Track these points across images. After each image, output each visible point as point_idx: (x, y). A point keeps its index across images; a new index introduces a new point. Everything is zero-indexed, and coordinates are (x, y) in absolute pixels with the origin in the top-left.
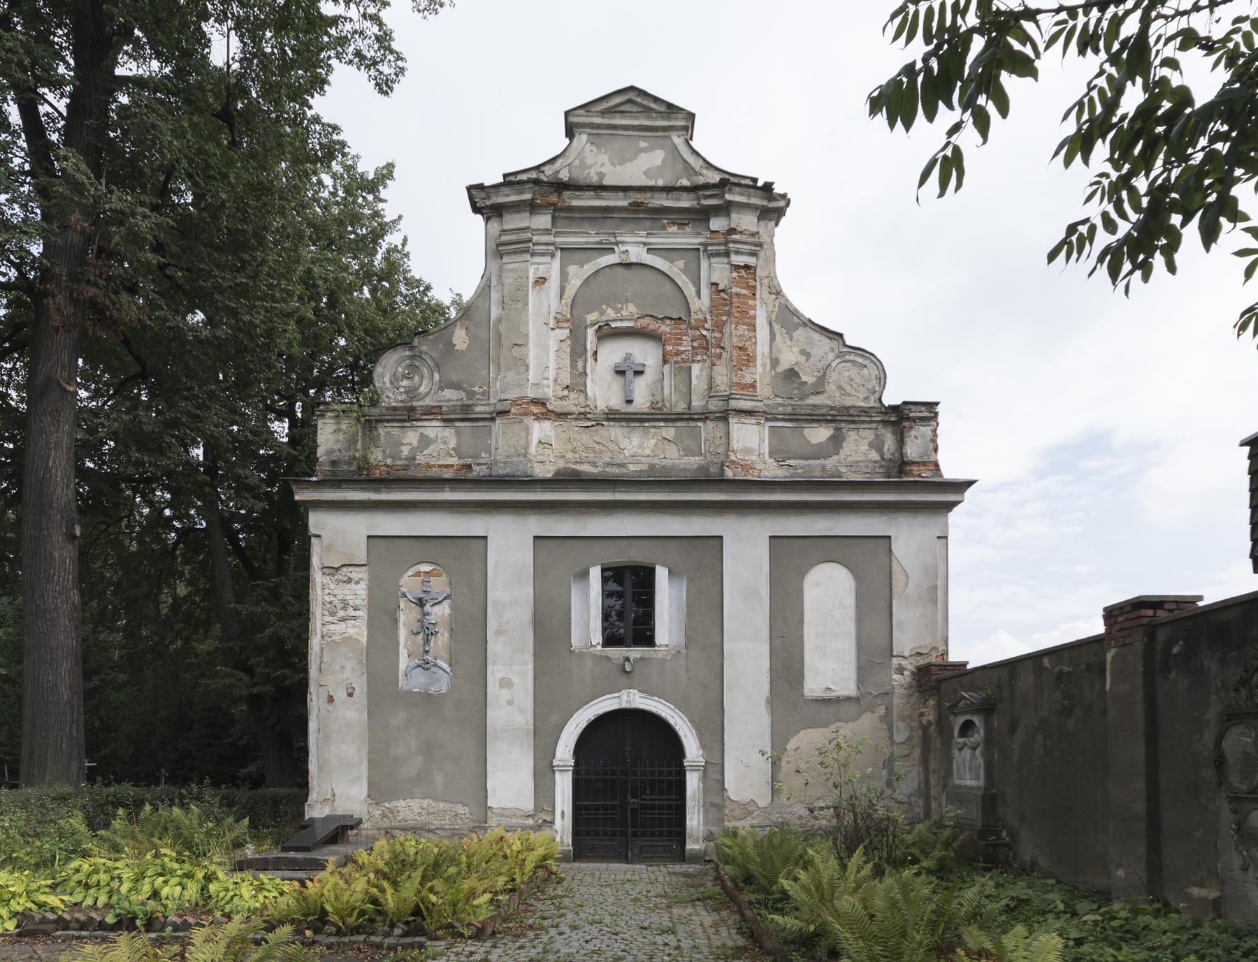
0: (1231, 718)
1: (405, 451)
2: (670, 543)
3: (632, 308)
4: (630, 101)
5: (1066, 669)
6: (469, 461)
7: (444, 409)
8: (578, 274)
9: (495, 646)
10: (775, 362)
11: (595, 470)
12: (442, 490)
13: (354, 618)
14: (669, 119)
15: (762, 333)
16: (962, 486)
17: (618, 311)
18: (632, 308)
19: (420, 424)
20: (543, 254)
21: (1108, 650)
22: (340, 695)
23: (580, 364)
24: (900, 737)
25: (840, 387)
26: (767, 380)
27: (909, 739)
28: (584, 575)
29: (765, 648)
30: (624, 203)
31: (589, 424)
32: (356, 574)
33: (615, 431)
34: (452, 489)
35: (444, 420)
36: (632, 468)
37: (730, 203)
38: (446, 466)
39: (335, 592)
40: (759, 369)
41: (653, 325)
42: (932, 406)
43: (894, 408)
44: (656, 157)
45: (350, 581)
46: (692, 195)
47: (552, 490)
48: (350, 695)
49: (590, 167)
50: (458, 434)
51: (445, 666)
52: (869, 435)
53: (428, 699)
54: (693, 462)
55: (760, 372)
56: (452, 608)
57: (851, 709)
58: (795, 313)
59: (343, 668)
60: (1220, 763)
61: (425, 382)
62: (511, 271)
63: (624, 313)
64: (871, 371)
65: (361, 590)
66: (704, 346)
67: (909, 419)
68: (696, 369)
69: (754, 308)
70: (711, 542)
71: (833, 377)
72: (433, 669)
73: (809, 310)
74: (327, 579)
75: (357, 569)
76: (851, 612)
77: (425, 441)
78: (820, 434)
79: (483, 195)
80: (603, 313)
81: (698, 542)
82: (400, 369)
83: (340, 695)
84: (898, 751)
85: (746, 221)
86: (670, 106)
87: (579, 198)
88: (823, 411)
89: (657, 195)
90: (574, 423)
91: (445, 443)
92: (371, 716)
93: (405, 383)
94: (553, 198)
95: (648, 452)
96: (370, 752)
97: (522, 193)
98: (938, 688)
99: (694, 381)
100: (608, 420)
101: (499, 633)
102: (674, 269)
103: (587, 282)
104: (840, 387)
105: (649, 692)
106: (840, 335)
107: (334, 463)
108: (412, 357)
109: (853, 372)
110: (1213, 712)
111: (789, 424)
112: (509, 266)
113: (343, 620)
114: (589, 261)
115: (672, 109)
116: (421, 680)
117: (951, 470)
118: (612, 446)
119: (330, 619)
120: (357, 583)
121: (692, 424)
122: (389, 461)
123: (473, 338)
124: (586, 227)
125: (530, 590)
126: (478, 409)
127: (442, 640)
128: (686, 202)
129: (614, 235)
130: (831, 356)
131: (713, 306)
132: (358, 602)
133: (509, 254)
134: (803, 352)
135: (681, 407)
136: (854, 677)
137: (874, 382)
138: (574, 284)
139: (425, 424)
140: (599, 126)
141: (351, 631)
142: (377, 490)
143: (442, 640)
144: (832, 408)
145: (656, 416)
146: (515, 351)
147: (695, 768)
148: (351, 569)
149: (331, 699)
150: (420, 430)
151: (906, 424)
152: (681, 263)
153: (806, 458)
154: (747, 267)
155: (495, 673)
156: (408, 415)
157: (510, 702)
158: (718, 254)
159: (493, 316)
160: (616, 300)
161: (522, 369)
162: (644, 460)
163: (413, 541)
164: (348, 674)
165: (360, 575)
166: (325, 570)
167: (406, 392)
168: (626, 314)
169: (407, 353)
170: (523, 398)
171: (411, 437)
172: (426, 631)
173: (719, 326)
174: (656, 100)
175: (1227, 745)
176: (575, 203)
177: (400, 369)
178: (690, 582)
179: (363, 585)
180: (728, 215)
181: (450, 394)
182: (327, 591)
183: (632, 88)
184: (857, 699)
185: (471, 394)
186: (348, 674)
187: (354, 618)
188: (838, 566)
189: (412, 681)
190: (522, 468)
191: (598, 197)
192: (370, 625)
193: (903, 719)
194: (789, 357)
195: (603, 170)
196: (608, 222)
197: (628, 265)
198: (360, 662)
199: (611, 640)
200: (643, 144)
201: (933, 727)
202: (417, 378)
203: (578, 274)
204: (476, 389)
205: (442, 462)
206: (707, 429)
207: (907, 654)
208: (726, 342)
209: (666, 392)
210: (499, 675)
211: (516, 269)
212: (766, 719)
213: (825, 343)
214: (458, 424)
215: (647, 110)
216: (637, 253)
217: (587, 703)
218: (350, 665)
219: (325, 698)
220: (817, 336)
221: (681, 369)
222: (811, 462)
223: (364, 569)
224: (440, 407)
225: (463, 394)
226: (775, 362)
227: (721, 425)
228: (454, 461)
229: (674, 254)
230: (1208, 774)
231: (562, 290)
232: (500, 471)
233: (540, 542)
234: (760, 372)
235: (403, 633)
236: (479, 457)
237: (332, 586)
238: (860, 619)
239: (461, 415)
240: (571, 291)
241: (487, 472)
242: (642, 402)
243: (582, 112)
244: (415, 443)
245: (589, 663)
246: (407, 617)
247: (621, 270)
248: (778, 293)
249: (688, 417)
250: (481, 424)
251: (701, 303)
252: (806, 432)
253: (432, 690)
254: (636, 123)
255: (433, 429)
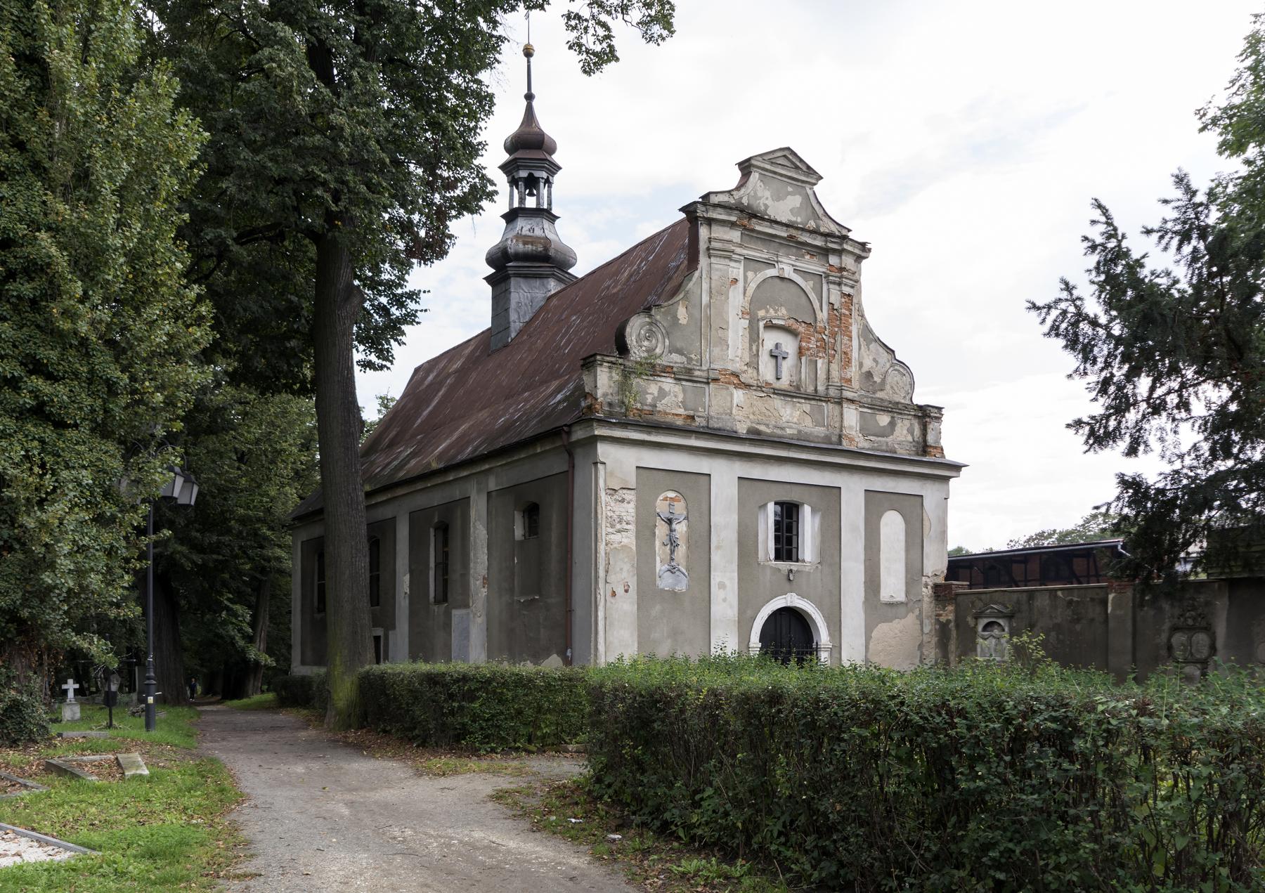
0: (1175, 629)
1: (649, 399)
2: (813, 488)
3: (783, 311)
4: (785, 156)
5: (1075, 599)
6: (691, 413)
7: (675, 369)
8: (756, 279)
9: (716, 557)
10: (861, 365)
11: (768, 431)
12: (690, 437)
13: (626, 531)
14: (808, 177)
15: (855, 343)
16: (957, 468)
17: (776, 311)
18: (783, 311)
19: (659, 379)
20: (736, 261)
21: (1111, 592)
22: (620, 590)
23: (754, 348)
24: (926, 630)
25: (892, 387)
26: (857, 377)
27: (931, 631)
28: (764, 506)
29: (862, 567)
30: (785, 235)
31: (763, 395)
32: (630, 496)
33: (777, 402)
34: (697, 438)
35: (676, 379)
36: (789, 431)
37: (844, 250)
38: (677, 415)
39: (615, 509)
40: (854, 369)
41: (795, 326)
42: (940, 409)
43: (920, 408)
44: (795, 201)
45: (623, 501)
46: (823, 238)
47: (755, 445)
48: (626, 591)
49: (760, 198)
50: (684, 391)
51: (684, 571)
52: (907, 423)
53: (674, 594)
54: (820, 431)
55: (853, 372)
56: (688, 527)
57: (902, 610)
58: (871, 332)
59: (621, 569)
60: (1170, 648)
61: (659, 345)
62: (717, 270)
63: (780, 314)
64: (907, 379)
65: (631, 508)
66: (823, 346)
67: (929, 417)
68: (820, 362)
69: (851, 324)
70: (835, 491)
71: (889, 380)
72: (677, 573)
73: (878, 333)
74: (608, 499)
75: (629, 492)
76: (903, 544)
77: (662, 393)
78: (884, 420)
79: (704, 209)
80: (767, 311)
81: (827, 490)
82: (642, 332)
83: (620, 590)
84: (926, 638)
85: (848, 261)
86: (809, 167)
87: (760, 224)
88: (886, 404)
89: (804, 234)
90: (754, 393)
91: (676, 396)
92: (638, 609)
93: (646, 343)
94: (745, 222)
95: (795, 420)
96: (639, 636)
97: (730, 215)
98: (955, 599)
99: (819, 372)
100: (774, 393)
101: (718, 547)
102: (807, 286)
103: (758, 287)
104: (892, 387)
105: (802, 595)
106: (893, 352)
107: (610, 404)
108: (650, 324)
109: (898, 378)
110: (1167, 626)
111: (869, 411)
112: (716, 266)
113: (619, 531)
114: (760, 270)
115: (810, 171)
116: (670, 581)
117: (951, 456)
118: (776, 413)
119: (610, 530)
120: (629, 503)
121: (820, 403)
122: (639, 405)
123: (690, 315)
124: (759, 246)
125: (735, 517)
126: (697, 373)
127: (682, 551)
128: (819, 242)
129: (777, 256)
130: (888, 365)
131: (830, 320)
132: (629, 518)
133: (716, 256)
134: (875, 360)
135: (810, 389)
136: (904, 589)
137: (908, 387)
138: (753, 286)
139: (663, 379)
140: (767, 170)
141: (625, 541)
142: (649, 433)
143: (682, 551)
144: (890, 402)
145: (793, 394)
146: (720, 331)
147: (826, 649)
148: (625, 491)
149: (614, 594)
150: (659, 384)
151: (928, 420)
152: (811, 283)
153: (878, 436)
154: (849, 295)
155: (716, 578)
156: (653, 370)
157: (725, 600)
158: (834, 283)
159: (704, 302)
160: (776, 303)
161: (725, 348)
162: (794, 426)
163: (664, 473)
164: (625, 574)
165: (631, 497)
166: (608, 491)
167: (647, 351)
168: (781, 315)
169: (647, 319)
170: (726, 370)
171: (653, 389)
172: (672, 543)
173: (833, 335)
174: (801, 160)
175: (1173, 640)
176: (758, 228)
177: (642, 332)
178: (823, 517)
179: (632, 505)
180: (840, 257)
181: (676, 357)
182: (609, 508)
183: (788, 149)
184: (907, 604)
185: (690, 360)
186: (625, 574)
187: (626, 531)
188: (900, 516)
189: (665, 582)
190: (729, 424)
191: (771, 227)
192: (637, 538)
193: (928, 617)
194: (868, 364)
195: (766, 202)
196: (773, 244)
197: (782, 279)
198: (633, 566)
199: (778, 557)
200: (790, 189)
201: (952, 625)
202: (654, 341)
203: (756, 279)
204: (693, 356)
205: (673, 412)
206: (829, 408)
207: (930, 575)
208: (838, 347)
209: (803, 376)
210: (718, 580)
211: (721, 270)
212: (862, 616)
213: (884, 356)
214: (684, 383)
215: (797, 167)
216: (788, 272)
217: (768, 602)
218: (627, 567)
219: (609, 593)
220: (881, 350)
221: (811, 360)
222: (880, 439)
223: (633, 492)
224: (672, 368)
225: (684, 359)
226: (861, 365)
227: (837, 407)
228: (681, 411)
229: (808, 276)
230: (1164, 652)
231: (745, 290)
232: (714, 424)
233: (742, 481)
234: (853, 372)
235: (658, 543)
236: (698, 411)
237: (612, 504)
238: (907, 550)
239: (684, 375)
240: (750, 291)
241: (704, 423)
242: (784, 383)
243: (760, 159)
244: (656, 394)
245: (768, 572)
246: (661, 530)
247: (778, 281)
248: (863, 316)
249: (814, 397)
250: (699, 385)
251: (823, 315)
252: (878, 417)
253: (678, 588)
254: (789, 174)
255: (668, 383)
